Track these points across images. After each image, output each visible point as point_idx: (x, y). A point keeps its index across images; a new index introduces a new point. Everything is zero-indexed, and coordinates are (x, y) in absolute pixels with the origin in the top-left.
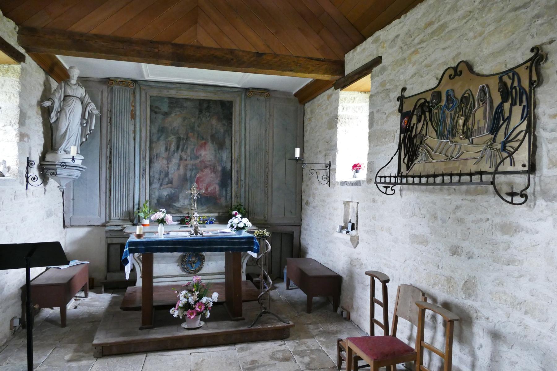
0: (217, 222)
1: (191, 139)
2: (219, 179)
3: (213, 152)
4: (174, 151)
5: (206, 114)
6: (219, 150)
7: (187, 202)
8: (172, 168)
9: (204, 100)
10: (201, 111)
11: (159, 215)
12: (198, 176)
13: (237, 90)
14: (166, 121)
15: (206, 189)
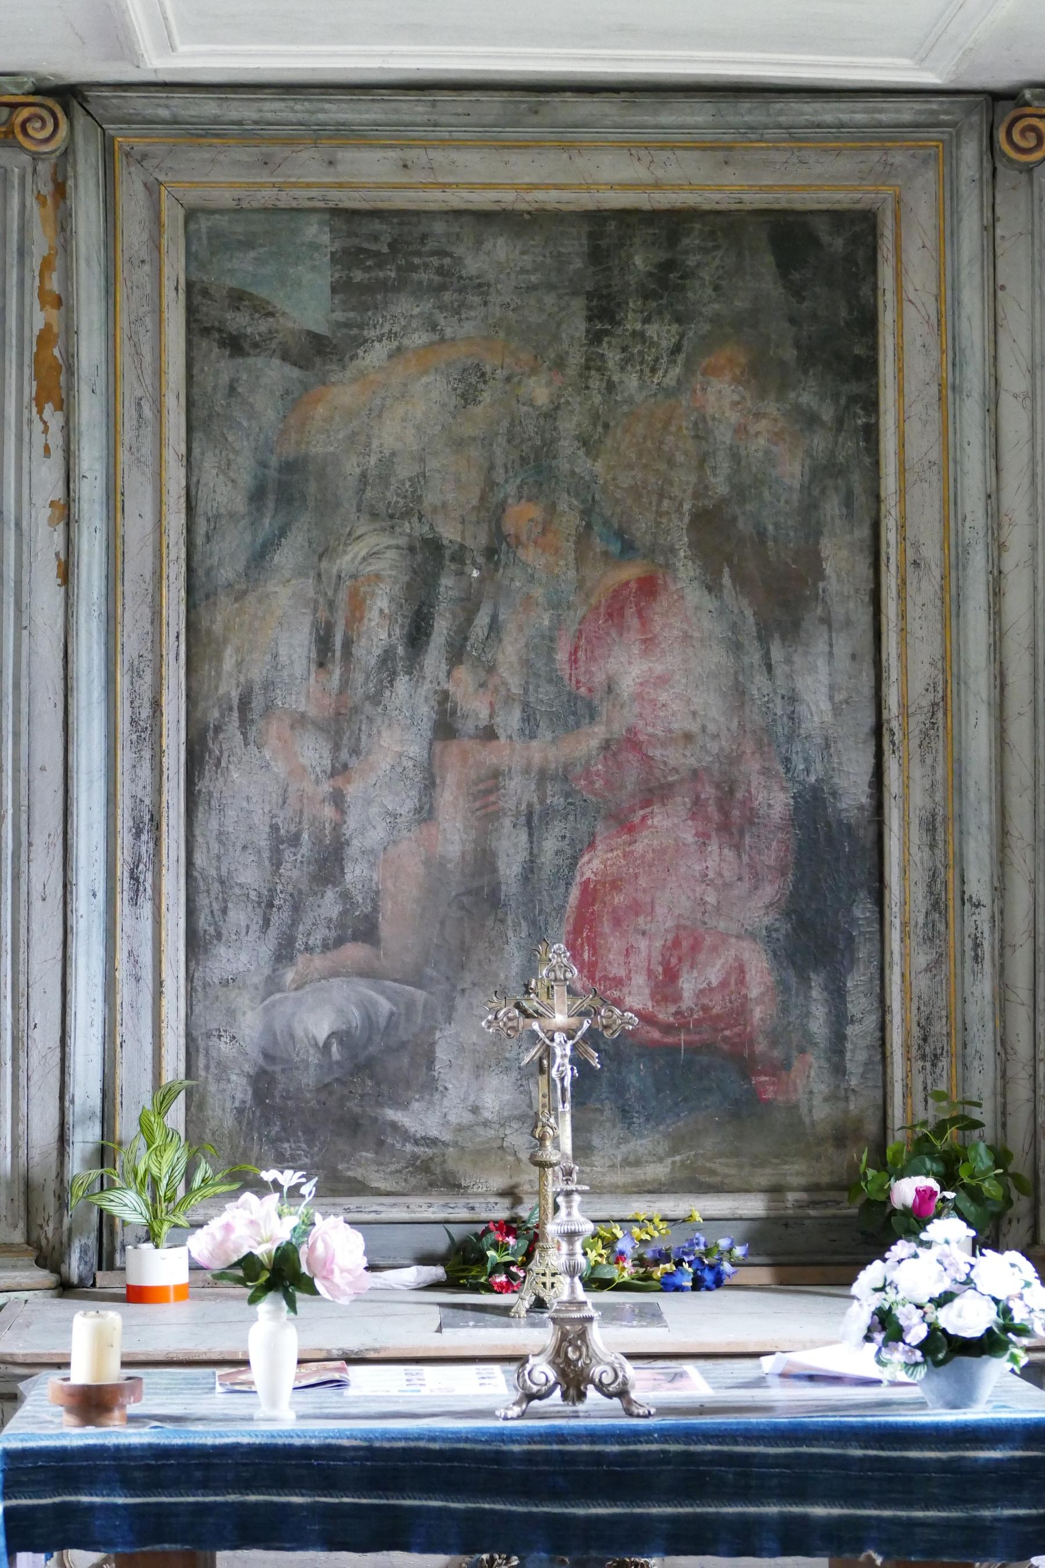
0: (763, 1275)
1: (529, 555)
2: (769, 891)
3: (717, 657)
4: (387, 657)
5: (652, 330)
6: (764, 639)
7: (496, 1095)
8: (376, 810)
9: (628, 218)
10: (604, 312)
11: (254, 1223)
12: (591, 867)
13: (907, 111)
14: (321, 410)
15: (666, 982)
